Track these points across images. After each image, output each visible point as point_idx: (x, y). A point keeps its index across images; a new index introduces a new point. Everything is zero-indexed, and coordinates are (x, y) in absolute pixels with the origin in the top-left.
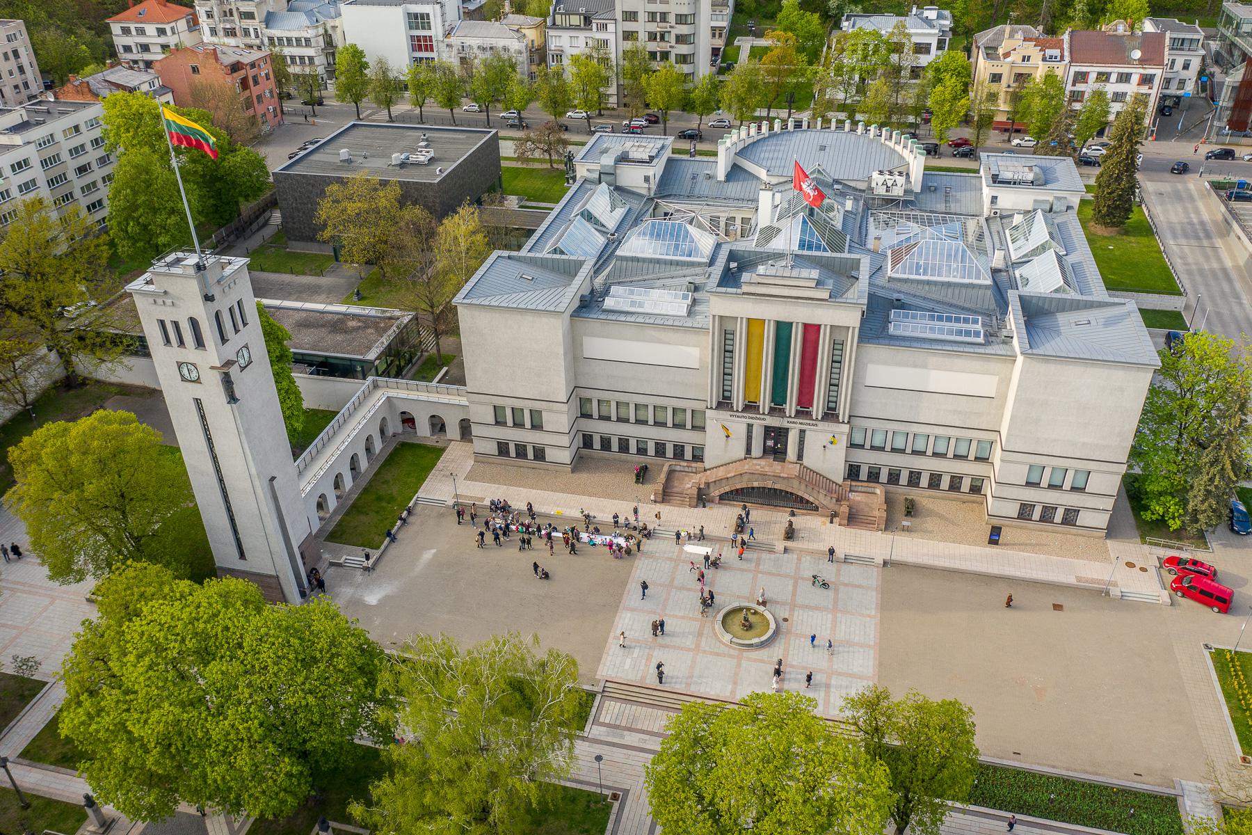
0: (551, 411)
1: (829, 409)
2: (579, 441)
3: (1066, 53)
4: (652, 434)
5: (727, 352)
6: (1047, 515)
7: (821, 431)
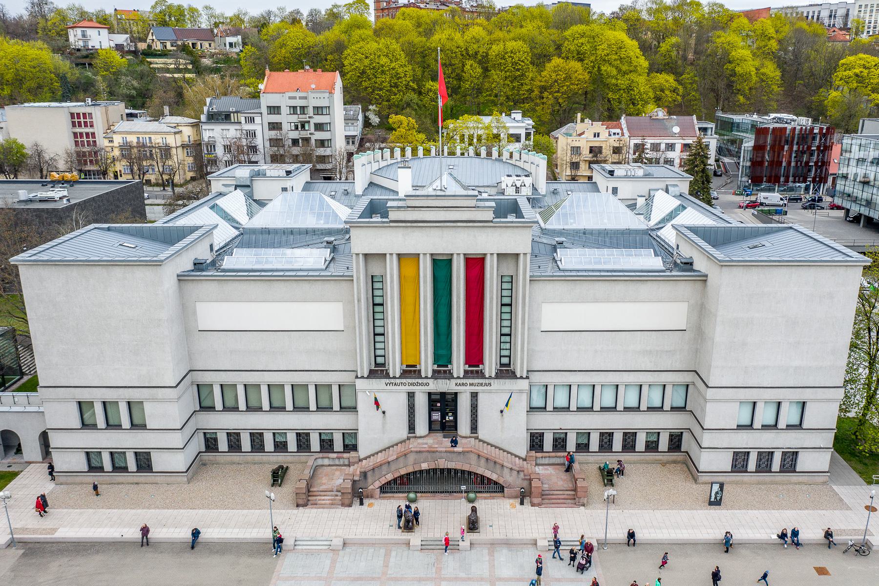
0: (154, 400)
1: (502, 365)
2: (198, 443)
3: (625, 131)
4: (290, 422)
5: (377, 305)
6: (765, 458)
7: (497, 391)
